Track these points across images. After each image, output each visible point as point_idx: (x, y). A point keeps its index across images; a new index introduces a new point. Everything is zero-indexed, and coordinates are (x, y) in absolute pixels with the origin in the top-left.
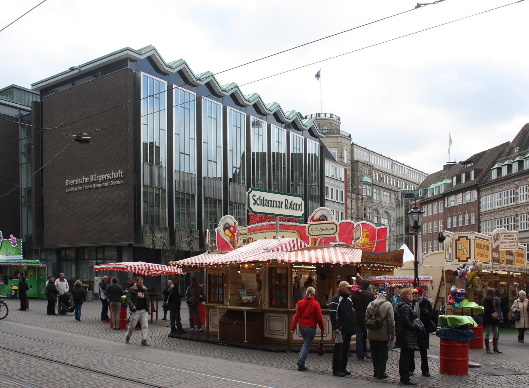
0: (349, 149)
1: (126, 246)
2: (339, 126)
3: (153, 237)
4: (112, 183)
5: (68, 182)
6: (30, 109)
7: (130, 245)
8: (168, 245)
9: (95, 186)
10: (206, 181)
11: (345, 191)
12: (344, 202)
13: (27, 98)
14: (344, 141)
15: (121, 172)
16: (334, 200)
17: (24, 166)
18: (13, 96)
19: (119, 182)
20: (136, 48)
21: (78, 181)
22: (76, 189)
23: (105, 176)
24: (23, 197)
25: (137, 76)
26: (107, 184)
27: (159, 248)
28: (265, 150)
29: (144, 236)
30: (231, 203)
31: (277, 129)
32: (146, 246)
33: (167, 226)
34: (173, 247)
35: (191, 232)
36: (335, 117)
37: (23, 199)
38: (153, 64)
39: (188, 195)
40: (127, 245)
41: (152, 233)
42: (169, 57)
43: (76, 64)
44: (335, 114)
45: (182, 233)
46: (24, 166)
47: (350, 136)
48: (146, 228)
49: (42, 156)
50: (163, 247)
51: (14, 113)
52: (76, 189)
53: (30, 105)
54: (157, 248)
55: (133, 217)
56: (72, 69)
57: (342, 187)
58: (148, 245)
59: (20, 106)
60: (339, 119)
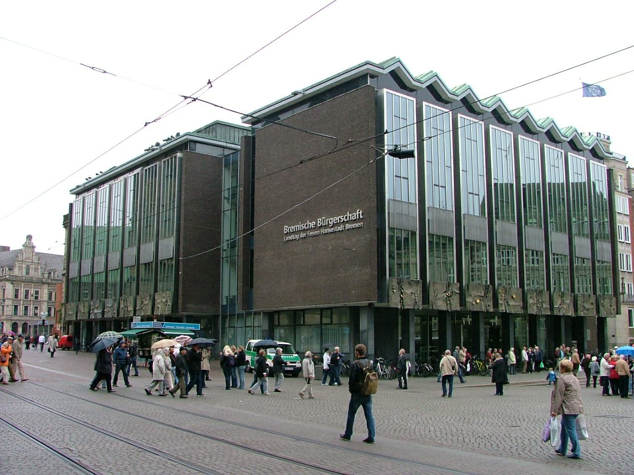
0: (624, 175)
1: (363, 307)
2: (608, 147)
3: (402, 292)
4: (348, 226)
5: (286, 229)
6: (239, 147)
7: (371, 305)
8: (421, 303)
9: (323, 231)
10: (466, 220)
11: (631, 226)
12: (630, 242)
13: (232, 135)
14: (617, 165)
15: (361, 212)
16: (623, 241)
17: (228, 213)
18: (216, 133)
19: (357, 225)
20: (377, 62)
21: (300, 226)
22: (297, 237)
23: (337, 218)
24: (225, 250)
25: (379, 94)
26: (340, 228)
27: (408, 307)
28: (538, 180)
29: (391, 293)
30: (499, 246)
31: (551, 151)
32: (392, 305)
33: (419, 279)
34: (426, 306)
35: (449, 285)
36: (602, 137)
37: (225, 253)
38: (399, 79)
39: (444, 237)
40: (367, 305)
41: (401, 288)
42: (417, 69)
43: (299, 88)
44: (602, 133)
45: (437, 286)
46: (228, 213)
47: (624, 158)
48: (392, 282)
49: (253, 200)
50: (414, 306)
51: (216, 153)
52: (297, 237)
53: (237, 141)
54: (406, 308)
55: (376, 268)
56: (295, 94)
57: (626, 223)
58: (395, 304)
59: (225, 144)
60: (608, 138)
